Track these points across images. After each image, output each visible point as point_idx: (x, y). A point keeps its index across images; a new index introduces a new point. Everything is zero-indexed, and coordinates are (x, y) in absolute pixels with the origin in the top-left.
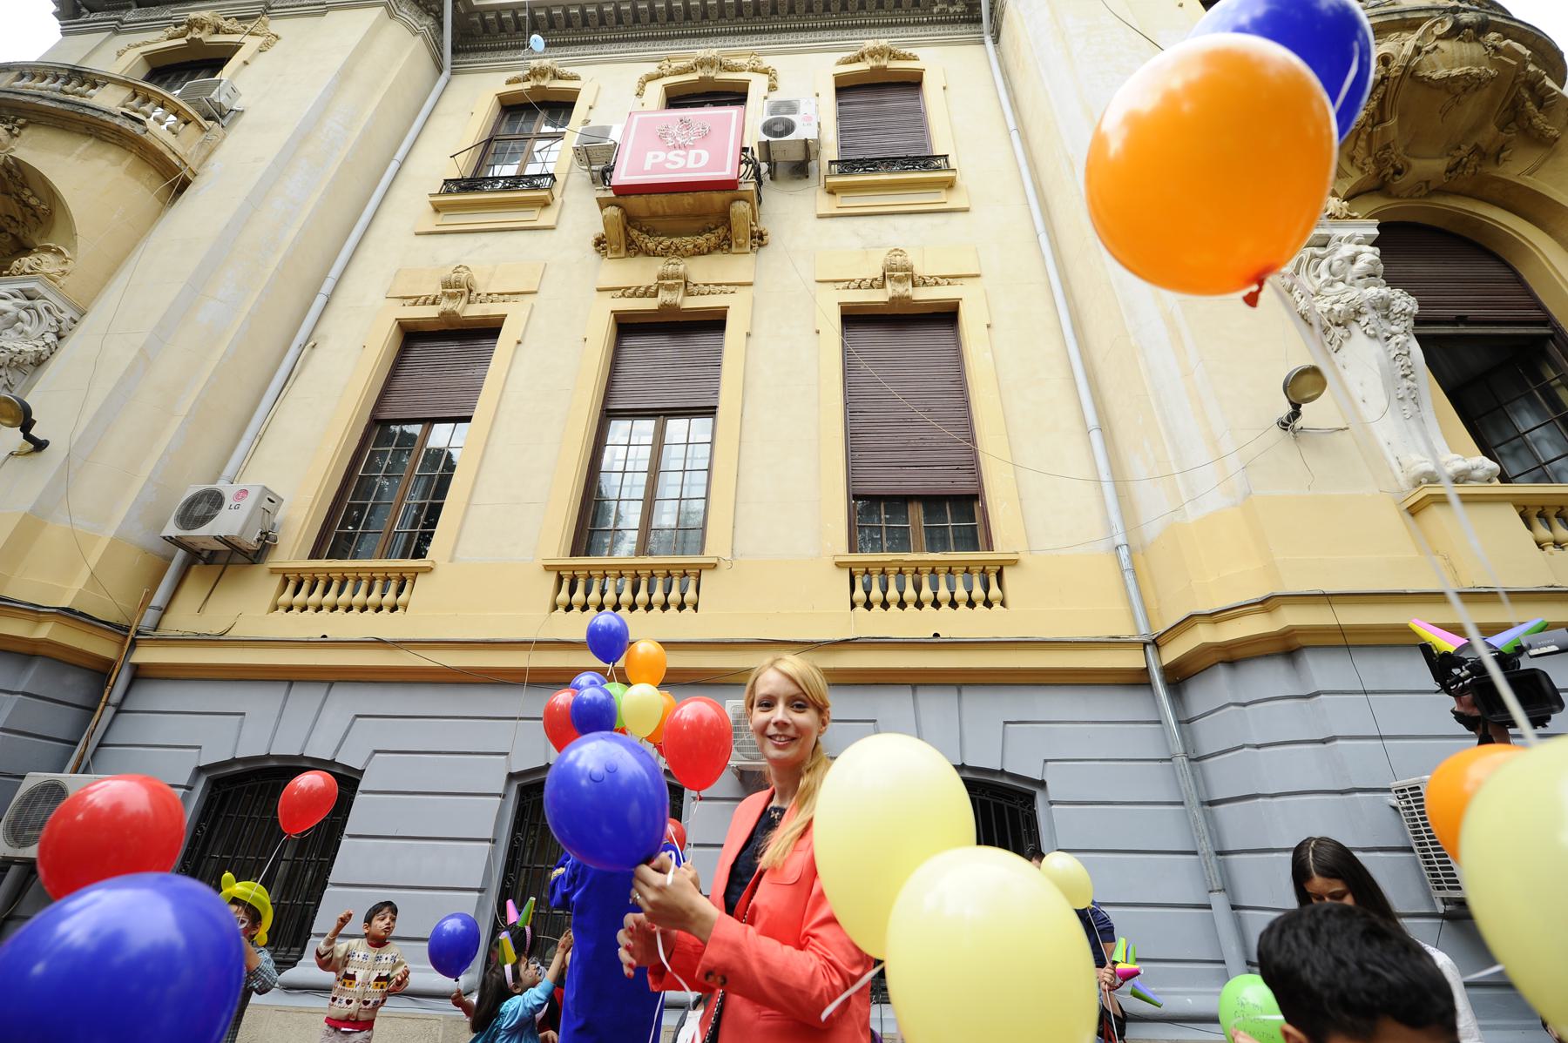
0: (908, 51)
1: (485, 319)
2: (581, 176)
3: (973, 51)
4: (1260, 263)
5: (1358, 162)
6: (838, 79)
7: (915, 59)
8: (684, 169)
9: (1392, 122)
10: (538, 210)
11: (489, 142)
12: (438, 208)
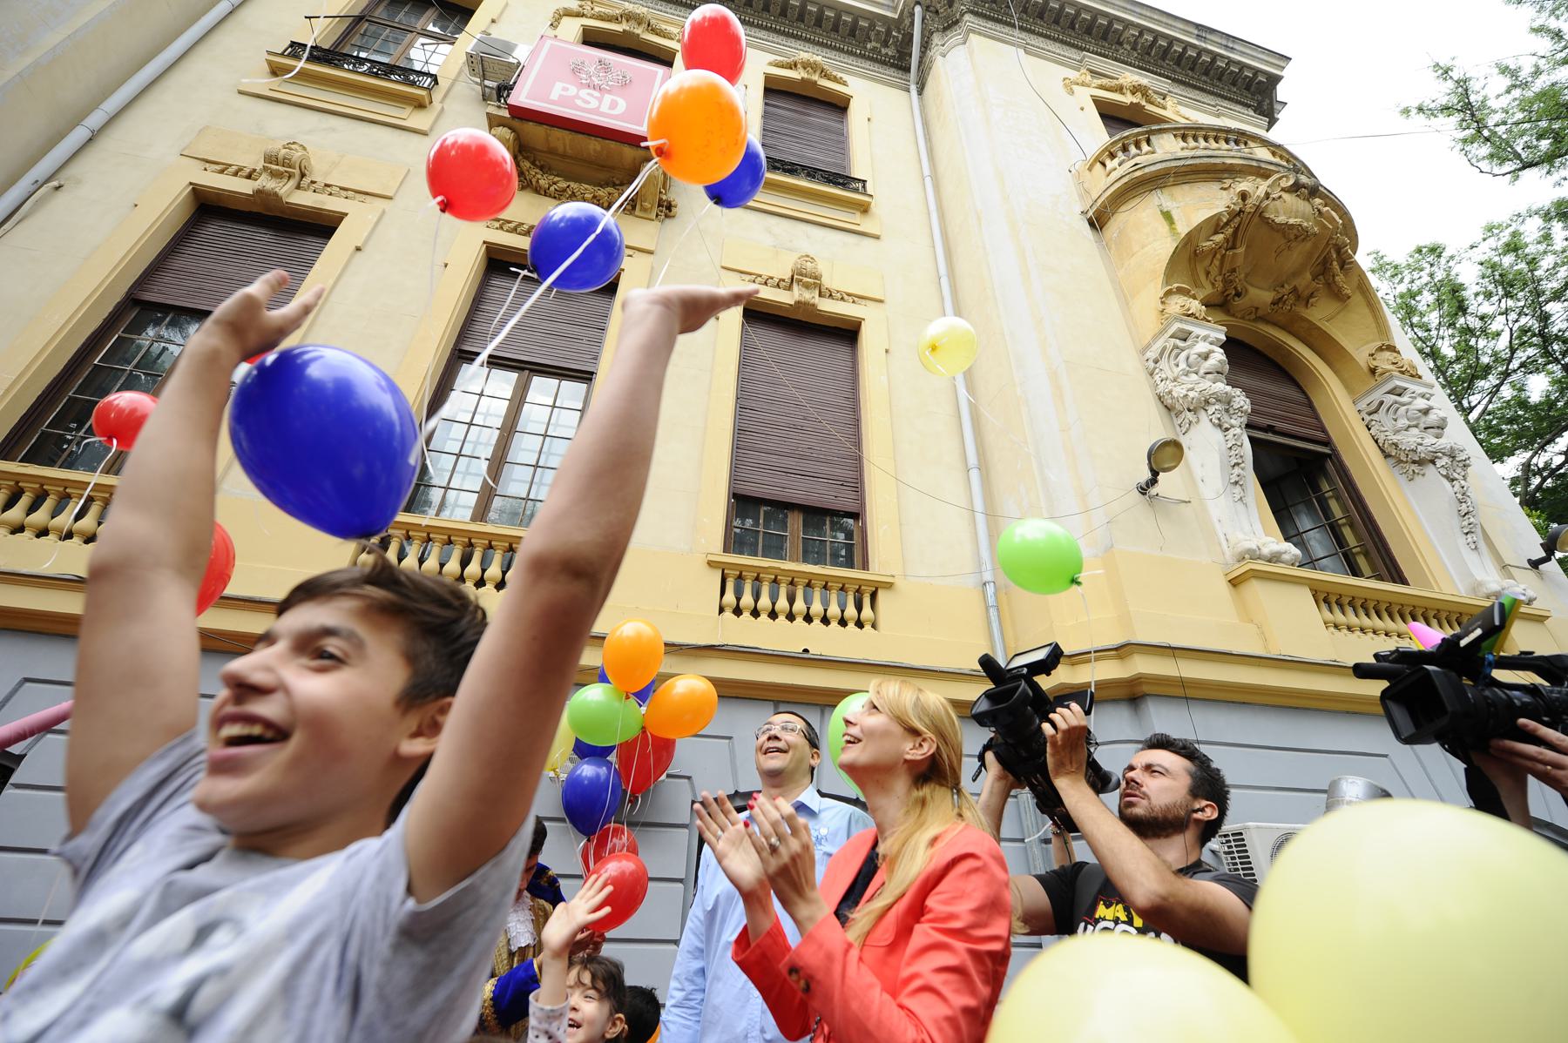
0: (840, 75)
1: (318, 213)
2: (469, 87)
3: (895, 95)
4: (60, 193)
5: (1211, 277)
6: (769, 79)
7: (845, 83)
8: (596, 111)
9: (1241, 250)
10: (409, 109)
11: (359, 19)
12: (276, 71)
